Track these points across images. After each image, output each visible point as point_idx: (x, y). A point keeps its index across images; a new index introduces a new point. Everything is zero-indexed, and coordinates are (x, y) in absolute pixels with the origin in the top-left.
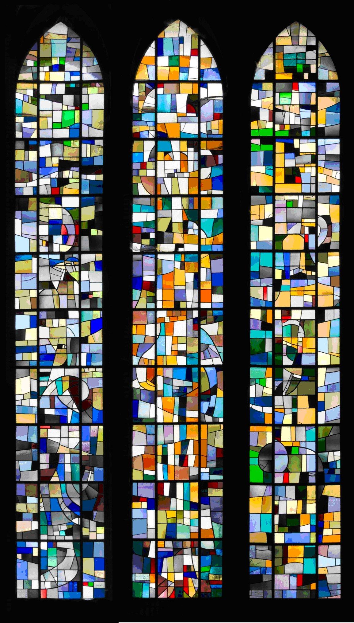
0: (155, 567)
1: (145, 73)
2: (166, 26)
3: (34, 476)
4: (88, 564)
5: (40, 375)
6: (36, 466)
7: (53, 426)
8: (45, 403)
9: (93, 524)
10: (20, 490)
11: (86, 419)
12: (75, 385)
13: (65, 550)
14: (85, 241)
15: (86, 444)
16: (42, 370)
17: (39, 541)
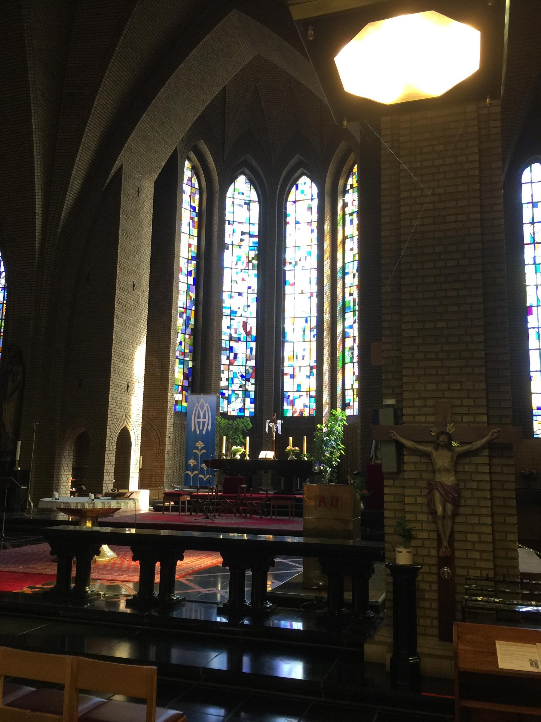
0: (292, 403)
1: (291, 197)
2: (237, 177)
3: (227, 362)
4: (248, 400)
5: (231, 319)
6: (228, 358)
7: (235, 341)
8: (233, 332)
9: (250, 384)
10: (222, 368)
11: (249, 339)
12: (245, 324)
13: (238, 395)
14: (250, 264)
15: (249, 350)
16: (232, 317)
17: (228, 390)
